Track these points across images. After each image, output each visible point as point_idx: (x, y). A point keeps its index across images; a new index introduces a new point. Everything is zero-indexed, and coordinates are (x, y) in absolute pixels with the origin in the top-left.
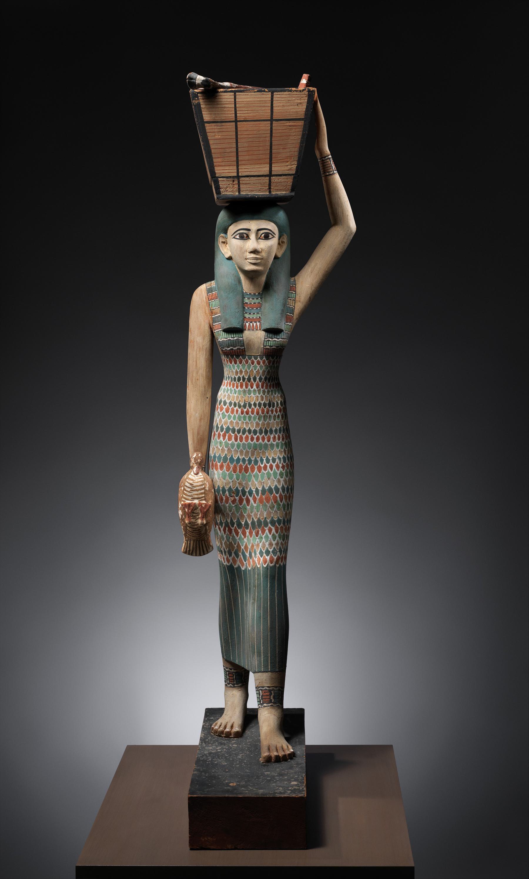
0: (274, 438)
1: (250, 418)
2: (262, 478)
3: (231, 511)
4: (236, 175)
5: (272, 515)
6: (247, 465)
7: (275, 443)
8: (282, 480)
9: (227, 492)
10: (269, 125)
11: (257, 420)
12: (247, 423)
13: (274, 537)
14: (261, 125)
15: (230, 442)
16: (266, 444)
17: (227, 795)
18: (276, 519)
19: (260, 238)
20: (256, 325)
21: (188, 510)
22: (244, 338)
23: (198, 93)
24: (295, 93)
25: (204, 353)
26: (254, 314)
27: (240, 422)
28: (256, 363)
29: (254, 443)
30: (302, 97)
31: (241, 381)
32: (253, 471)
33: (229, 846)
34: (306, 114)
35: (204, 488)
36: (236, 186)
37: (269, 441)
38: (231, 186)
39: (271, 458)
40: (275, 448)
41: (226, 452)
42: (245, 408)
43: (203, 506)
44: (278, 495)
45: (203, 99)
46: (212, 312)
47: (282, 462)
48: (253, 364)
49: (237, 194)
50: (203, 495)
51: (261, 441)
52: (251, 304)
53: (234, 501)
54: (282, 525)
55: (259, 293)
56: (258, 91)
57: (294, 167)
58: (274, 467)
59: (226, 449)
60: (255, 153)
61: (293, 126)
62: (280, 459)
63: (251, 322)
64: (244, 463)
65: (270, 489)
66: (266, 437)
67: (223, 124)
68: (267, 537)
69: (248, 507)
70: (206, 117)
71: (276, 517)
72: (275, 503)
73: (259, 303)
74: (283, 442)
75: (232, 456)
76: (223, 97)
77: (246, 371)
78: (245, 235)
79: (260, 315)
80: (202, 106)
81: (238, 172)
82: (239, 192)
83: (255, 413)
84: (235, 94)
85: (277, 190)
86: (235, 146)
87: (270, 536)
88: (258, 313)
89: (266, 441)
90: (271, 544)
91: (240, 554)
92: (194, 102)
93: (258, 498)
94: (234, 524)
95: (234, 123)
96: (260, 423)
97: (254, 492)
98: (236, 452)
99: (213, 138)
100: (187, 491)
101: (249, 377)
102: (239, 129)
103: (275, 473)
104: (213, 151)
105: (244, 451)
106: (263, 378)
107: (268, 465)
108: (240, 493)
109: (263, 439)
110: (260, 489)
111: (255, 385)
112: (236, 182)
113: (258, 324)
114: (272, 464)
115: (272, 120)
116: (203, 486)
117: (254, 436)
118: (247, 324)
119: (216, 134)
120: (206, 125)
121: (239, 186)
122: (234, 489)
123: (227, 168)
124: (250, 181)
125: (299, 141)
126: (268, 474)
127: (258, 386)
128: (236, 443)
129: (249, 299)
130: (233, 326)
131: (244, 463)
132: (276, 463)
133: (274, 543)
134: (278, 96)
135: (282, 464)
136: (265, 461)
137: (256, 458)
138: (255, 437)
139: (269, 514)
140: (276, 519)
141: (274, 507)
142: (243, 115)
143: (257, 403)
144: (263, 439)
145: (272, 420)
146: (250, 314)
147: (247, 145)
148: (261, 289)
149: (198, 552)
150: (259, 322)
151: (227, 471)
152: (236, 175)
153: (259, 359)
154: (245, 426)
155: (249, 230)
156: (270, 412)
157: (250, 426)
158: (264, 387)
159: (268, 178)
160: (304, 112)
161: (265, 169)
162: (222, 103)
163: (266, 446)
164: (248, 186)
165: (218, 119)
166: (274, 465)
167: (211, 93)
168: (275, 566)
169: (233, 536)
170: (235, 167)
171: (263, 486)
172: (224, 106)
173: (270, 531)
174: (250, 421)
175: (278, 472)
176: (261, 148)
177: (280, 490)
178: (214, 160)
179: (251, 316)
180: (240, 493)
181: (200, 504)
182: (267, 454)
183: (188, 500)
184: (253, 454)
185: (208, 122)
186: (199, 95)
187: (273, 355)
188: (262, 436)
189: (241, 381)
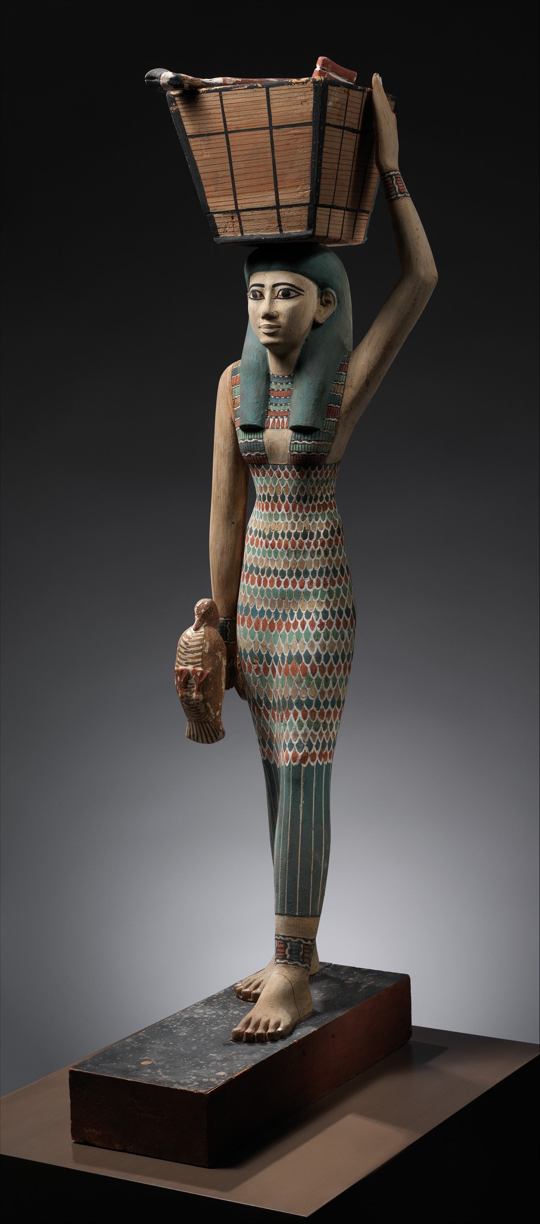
0: (311, 584)
1: (276, 553)
2: (290, 639)
3: (256, 684)
4: (234, 209)
5: (299, 694)
6: (272, 620)
7: (311, 590)
8: (317, 644)
9: (249, 657)
10: (269, 135)
11: (285, 556)
12: (272, 560)
13: (301, 726)
14: (258, 136)
15: (253, 587)
16: (297, 591)
17: (115, 1076)
18: (304, 700)
19: (277, 297)
20: (283, 421)
21: (180, 679)
22: (265, 440)
23: (175, 96)
24: (296, 86)
25: (227, 461)
26: (281, 405)
27: (264, 559)
28: (283, 475)
29: (282, 589)
30: (307, 92)
31: (267, 500)
32: (280, 629)
33: (117, 1146)
34: (314, 116)
35: (201, 650)
36: (237, 224)
37: (302, 587)
38: (231, 224)
39: (304, 612)
40: (312, 597)
41: (248, 601)
42: (270, 539)
43: (199, 674)
44: (308, 666)
45: (182, 104)
46: (234, 404)
47: (321, 617)
48: (279, 477)
49: (240, 235)
50: (200, 660)
51: (290, 586)
52: (278, 390)
53: (258, 670)
54: (313, 708)
55: (289, 376)
56: (248, 88)
57: (307, 193)
58: (307, 625)
59: (248, 596)
60: (255, 177)
61: (299, 134)
62: (317, 613)
63: (276, 417)
64: (269, 617)
65: (298, 656)
66: (298, 582)
67: (211, 137)
68: (291, 724)
69: (274, 680)
70: (190, 129)
71: (304, 696)
72: (304, 676)
73: (289, 389)
74: (326, 590)
75: (255, 606)
76: (206, 99)
77: (271, 486)
78: (258, 294)
79: (288, 407)
80: (182, 114)
81: (236, 205)
82: (242, 232)
83: (283, 547)
84: (220, 94)
85: (290, 228)
86: (229, 168)
87: (295, 723)
88: (286, 404)
89: (298, 587)
90: (296, 735)
91: (274, 745)
92: (172, 109)
93: (283, 667)
94: (262, 702)
95: (224, 136)
96: (290, 561)
97: (280, 659)
98: (260, 600)
99: (201, 158)
100: (181, 652)
101: (276, 494)
102: (231, 143)
103: (307, 634)
104: (202, 176)
105: (269, 600)
106: (295, 496)
107: (299, 621)
108: (265, 660)
109: (294, 584)
110: (286, 655)
111: (283, 506)
112: (236, 219)
113: (285, 419)
114: (305, 619)
115: (271, 128)
116: (201, 647)
117: (281, 579)
118: (271, 420)
119: (204, 152)
120: (190, 140)
121: (240, 224)
122: (256, 653)
123: (222, 199)
124: (254, 217)
125: (310, 155)
126: (298, 634)
127: (287, 509)
128: (259, 588)
129: (276, 383)
130: (248, 423)
131: (269, 617)
132: (311, 619)
133: (300, 733)
134: (276, 92)
135: (321, 621)
136: (296, 615)
137: (284, 611)
138: (283, 580)
139: (295, 691)
140: (304, 700)
141: (301, 682)
142: (233, 123)
143: (286, 532)
144: (294, 584)
145: (308, 558)
146: (276, 405)
147: (243, 166)
148: (292, 370)
149: (209, 739)
150: (287, 416)
151: (249, 627)
152: (234, 209)
153: (286, 469)
154: (270, 565)
155: (262, 286)
156: (305, 546)
157: (276, 565)
158: (297, 511)
159: (276, 211)
160: (311, 114)
161: (269, 199)
162: (206, 107)
163: (298, 593)
164: (252, 223)
165: (204, 131)
166: (308, 622)
167: (191, 96)
168: (299, 766)
169: (263, 719)
170: (232, 198)
171: (290, 652)
172: (208, 112)
173: (296, 715)
174: (276, 557)
175: (313, 632)
176: (261, 169)
177: (313, 658)
178: (206, 189)
179: (277, 409)
180: (265, 660)
181: (195, 672)
182: (299, 606)
183: (181, 665)
184: (280, 605)
185: (193, 136)
186: (176, 98)
187: (305, 463)
188: (292, 579)
189: (267, 500)
